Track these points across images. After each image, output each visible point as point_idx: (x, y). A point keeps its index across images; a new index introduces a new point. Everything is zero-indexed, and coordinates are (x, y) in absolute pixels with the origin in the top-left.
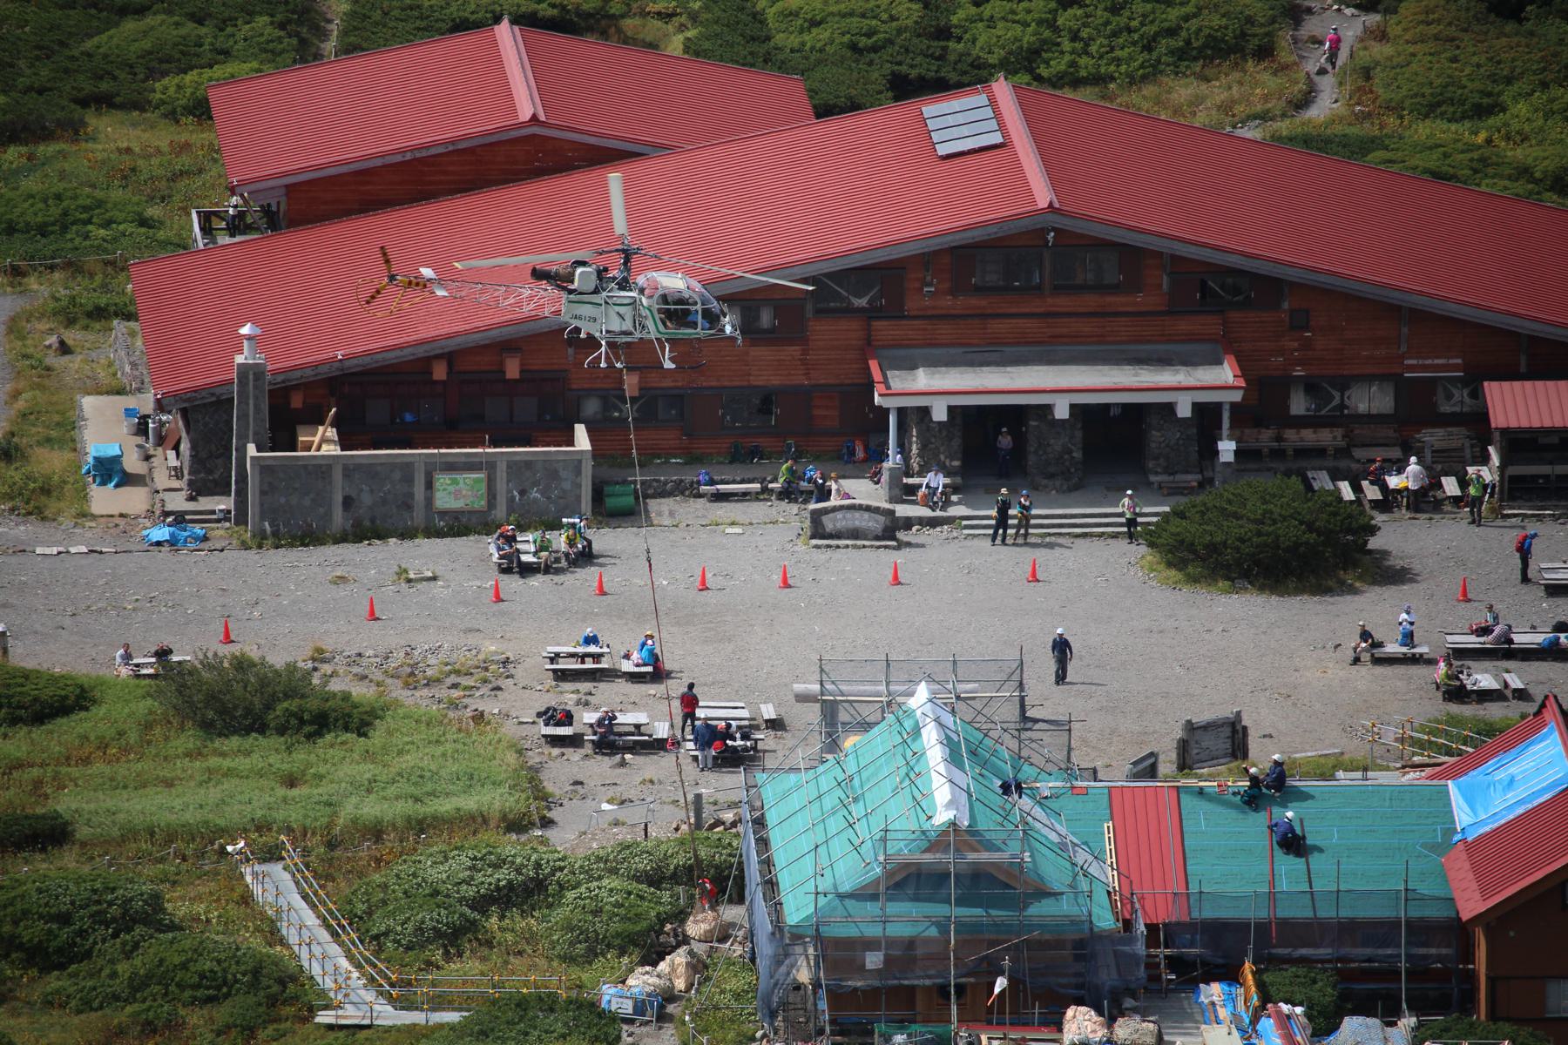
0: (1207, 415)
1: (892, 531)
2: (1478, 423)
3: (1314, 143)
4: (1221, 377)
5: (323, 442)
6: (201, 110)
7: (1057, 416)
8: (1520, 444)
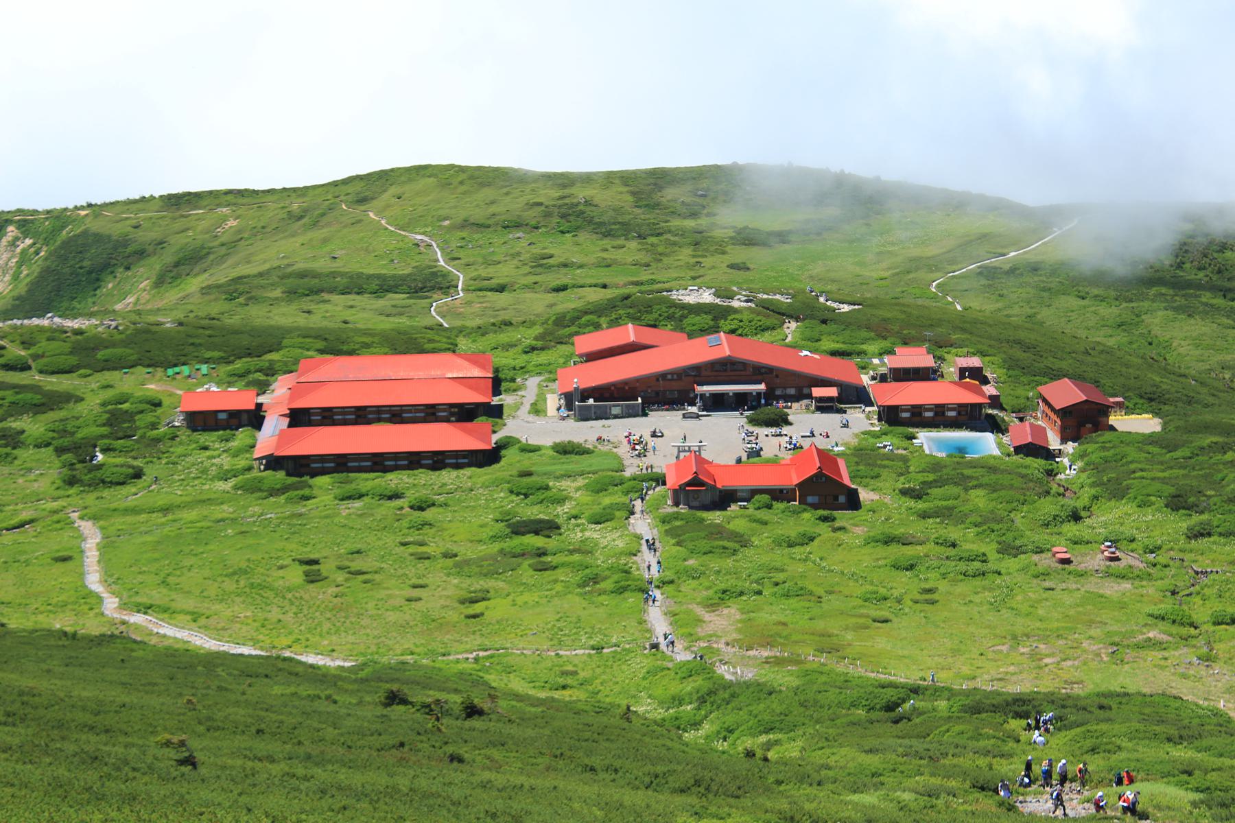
0: (759, 394)
1: (698, 417)
2: (810, 396)
3: (787, 346)
4: (762, 387)
5: (591, 401)
6: (573, 344)
7: (1158, 429)
8: (820, 400)
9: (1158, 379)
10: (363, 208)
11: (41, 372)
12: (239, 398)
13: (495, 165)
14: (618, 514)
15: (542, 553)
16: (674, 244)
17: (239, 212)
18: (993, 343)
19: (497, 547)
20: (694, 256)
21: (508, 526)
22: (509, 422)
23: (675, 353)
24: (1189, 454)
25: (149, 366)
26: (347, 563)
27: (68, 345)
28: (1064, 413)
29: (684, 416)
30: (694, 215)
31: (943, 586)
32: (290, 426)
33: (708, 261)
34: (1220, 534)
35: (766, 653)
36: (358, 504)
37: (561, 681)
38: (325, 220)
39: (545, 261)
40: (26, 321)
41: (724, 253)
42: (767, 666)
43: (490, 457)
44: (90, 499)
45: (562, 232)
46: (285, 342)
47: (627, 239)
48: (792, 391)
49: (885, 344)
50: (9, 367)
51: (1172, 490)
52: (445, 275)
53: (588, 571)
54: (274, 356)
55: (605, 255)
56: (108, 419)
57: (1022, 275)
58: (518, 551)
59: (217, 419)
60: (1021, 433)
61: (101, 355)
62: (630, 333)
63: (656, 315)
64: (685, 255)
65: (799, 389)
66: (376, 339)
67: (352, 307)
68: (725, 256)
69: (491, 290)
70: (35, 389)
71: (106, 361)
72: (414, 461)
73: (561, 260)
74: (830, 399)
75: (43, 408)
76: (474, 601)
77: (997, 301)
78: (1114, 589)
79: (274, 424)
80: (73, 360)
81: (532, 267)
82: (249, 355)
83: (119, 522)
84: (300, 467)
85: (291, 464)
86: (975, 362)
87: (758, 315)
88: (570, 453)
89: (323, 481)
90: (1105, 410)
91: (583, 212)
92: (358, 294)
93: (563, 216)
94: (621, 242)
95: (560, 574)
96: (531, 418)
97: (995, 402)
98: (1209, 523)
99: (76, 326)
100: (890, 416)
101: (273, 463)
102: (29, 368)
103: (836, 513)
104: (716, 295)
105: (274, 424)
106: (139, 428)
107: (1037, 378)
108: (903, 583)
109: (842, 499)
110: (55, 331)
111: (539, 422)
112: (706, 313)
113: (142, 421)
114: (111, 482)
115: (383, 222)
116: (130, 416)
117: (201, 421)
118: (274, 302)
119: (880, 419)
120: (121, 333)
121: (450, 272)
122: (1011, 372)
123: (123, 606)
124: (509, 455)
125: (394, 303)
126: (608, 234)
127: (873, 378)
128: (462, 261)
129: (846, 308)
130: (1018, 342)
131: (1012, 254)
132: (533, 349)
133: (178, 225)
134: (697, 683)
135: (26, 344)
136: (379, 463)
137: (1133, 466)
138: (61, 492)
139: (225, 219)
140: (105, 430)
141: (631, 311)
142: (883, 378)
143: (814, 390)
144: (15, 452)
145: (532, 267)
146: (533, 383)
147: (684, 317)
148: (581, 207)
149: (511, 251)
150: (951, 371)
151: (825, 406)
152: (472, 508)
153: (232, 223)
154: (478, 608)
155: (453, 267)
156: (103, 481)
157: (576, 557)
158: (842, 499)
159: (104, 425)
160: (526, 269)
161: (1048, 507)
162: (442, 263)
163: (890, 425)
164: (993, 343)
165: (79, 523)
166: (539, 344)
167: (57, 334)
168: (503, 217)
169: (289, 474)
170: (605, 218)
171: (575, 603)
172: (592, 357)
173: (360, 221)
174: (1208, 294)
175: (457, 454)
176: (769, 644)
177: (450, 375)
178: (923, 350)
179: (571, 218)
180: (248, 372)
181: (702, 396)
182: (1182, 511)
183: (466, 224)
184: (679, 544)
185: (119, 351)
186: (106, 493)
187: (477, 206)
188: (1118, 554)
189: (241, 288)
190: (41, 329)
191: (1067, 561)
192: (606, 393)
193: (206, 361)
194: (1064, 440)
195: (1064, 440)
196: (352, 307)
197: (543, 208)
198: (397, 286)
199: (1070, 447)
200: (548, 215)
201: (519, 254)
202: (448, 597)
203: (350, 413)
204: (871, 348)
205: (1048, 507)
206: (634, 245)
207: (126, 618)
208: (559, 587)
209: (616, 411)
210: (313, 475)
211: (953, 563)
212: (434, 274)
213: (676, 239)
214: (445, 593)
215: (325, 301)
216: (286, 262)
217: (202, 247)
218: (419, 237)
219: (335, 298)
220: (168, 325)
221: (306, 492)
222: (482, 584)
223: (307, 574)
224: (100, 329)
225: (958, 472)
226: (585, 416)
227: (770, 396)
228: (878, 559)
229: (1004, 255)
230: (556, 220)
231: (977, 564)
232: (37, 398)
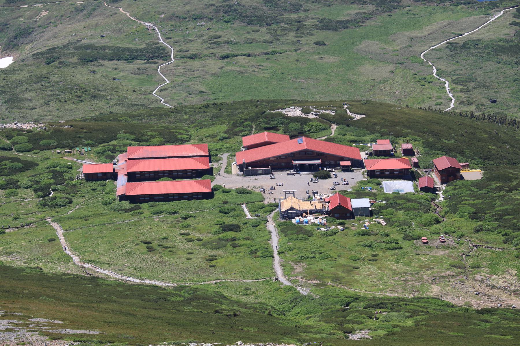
0: (319, 165)
1: (293, 174)
4: (319, 161)
5: (250, 168)
8: (343, 166)
10: (116, 5)
11: (18, 151)
12: (107, 168)
14: (262, 222)
15: (234, 239)
16: (286, 29)
17: (48, 7)
19: (217, 237)
20: (296, 37)
21: (221, 227)
22: (217, 176)
23: (285, 146)
24: (486, 192)
26: (162, 243)
29: (288, 174)
30: (296, 11)
31: (381, 254)
33: (304, 40)
34: (485, 230)
35: (315, 282)
36: (161, 216)
37: (245, 292)
38: (96, 13)
39: (216, 40)
41: (312, 35)
42: (314, 287)
44: (53, 212)
45: (226, 22)
46: (118, 136)
47: (260, 26)
48: (333, 163)
49: (373, 136)
50: (4, 149)
51: (473, 210)
52: (164, 49)
53: (252, 248)
54: (114, 143)
55: (249, 36)
56: (52, 175)
57: (469, 48)
58: (225, 238)
60: (423, 182)
61: (42, 142)
62: (265, 136)
63: (276, 122)
64: (292, 36)
65: (336, 162)
66: (156, 133)
67: (116, 69)
68: (313, 37)
69: (189, 58)
70: (18, 160)
71: (44, 146)
72: (180, 197)
73: (226, 39)
74: (348, 166)
75: (23, 169)
76: (211, 260)
77: (454, 65)
78: (441, 253)
79: (122, 180)
80: (30, 146)
81: (210, 44)
82: (104, 142)
83: (69, 223)
84: (136, 200)
86: (409, 146)
87: (320, 122)
88: (243, 193)
89: (144, 205)
90: (458, 170)
91: (236, 10)
92: (118, 60)
93: (226, 12)
94: (257, 27)
95: (242, 249)
96: (226, 175)
97: (416, 165)
98: (482, 226)
99: (28, 128)
101: (123, 198)
102: (12, 149)
103: (346, 221)
104: (303, 111)
105: (122, 180)
106: (66, 180)
107: (437, 151)
108: (368, 253)
109: (348, 215)
110: (20, 130)
111: (229, 177)
112: (297, 122)
113: (67, 176)
114: (60, 205)
115: (128, 14)
116: (60, 174)
117: (91, 177)
118: (75, 65)
119: (367, 175)
120: (47, 131)
121: (166, 47)
122: (426, 149)
123: (82, 260)
124: (218, 195)
125: (138, 66)
126: (250, 23)
127: (367, 154)
128: (172, 40)
130: (432, 133)
131: (466, 34)
132: (224, 138)
133: (14, 15)
134: (289, 296)
135: (9, 137)
136: (167, 198)
137: (463, 198)
138: (40, 210)
139: (40, 11)
140: (52, 181)
141: (265, 120)
143: (341, 162)
144: (17, 190)
145: (210, 44)
146: (225, 156)
147: (288, 123)
148: (235, 7)
149: (199, 33)
150: (400, 152)
151: (346, 169)
152: (205, 220)
153: (44, 13)
154: (213, 263)
155: (168, 43)
156: (57, 205)
157: (248, 242)
158: (348, 215)
159: (51, 178)
160: (207, 45)
161: (426, 217)
162: (162, 41)
163: (371, 178)
165: (52, 223)
166: (226, 135)
168: (193, 13)
170: (248, 14)
171: (249, 261)
172: (249, 148)
173: (115, 14)
175: (197, 194)
176: (316, 279)
178: (388, 141)
179: (230, 13)
180: (105, 151)
181: (296, 165)
182: (475, 220)
183: (173, 17)
184: (285, 236)
186: (59, 209)
187: (179, 6)
188: (445, 240)
189: (55, 55)
191: (427, 243)
192: (256, 164)
193: (86, 145)
194: (442, 183)
195: (442, 183)
196: (116, 69)
197: (214, 7)
198: (138, 56)
199: (443, 187)
200: (217, 11)
201: (202, 36)
202: (201, 258)
204: (368, 138)
205: (426, 217)
206: (264, 29)
207: (84, 265)
208: (242, 254)
209: (260, 172)
210: (141, 202)
211: (385, 244)
212: (158, 48)
213: (287, 26)
214: (200, 256)
215: (101, 65)
216: (76, 38)
217: (29, 28)
218: (148, 24)
219: (106, 63)
221: (139, 211)
222: (214, 252)
223: (148, 248)
224: (38, 130)
225: (397, 200)
226: (248, 174)
227: (323, 165)
228: (359, 242)
229: (461, 35)
230: (222, 14)
231: (394, 244)
232: (20, 165)
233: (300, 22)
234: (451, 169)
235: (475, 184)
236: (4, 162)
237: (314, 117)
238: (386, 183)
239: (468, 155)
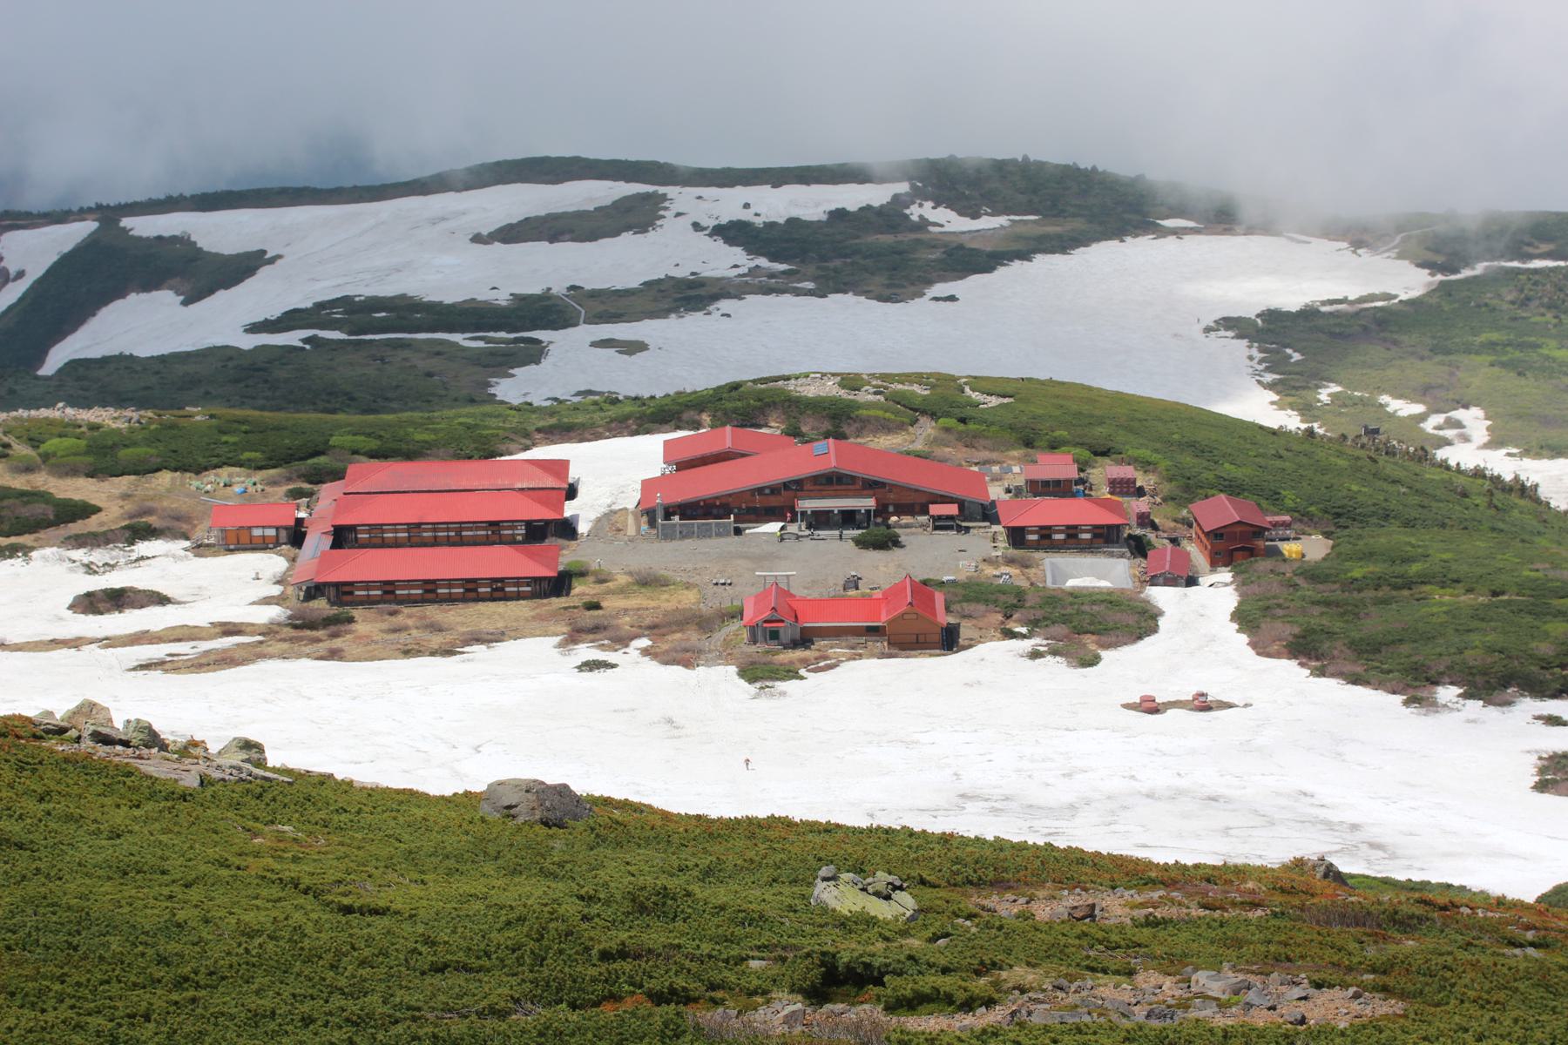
0: (868, 512)
5: (676, 518)
8: (940, 518)
9: (1355, 488)
13: (632, 158)
18: (1158, 445)
20: (888, 286)
25: (175, 470)
27: (83, 443)
28: (1216, 534)
32: (332, 547)
39: (692, 293)
40: (33, 412)
43: (559, 585)
59: (251, 537)
85: (333, 592)
97: (1145, 520)
99: (93, 419)
100: (1017, 536)
104: (842, 385)
110: (67, 425)
127: (1008, 491)
129: (994, 401)
130: (1192, 445)
135: (34, 442)
142: (1018, 492)
151: (941, 524)
164: (1158, 445)
167: (70, 429)
169: (332, 604)
174: (1553, 343)
177: (519, 485)
185: (141, 451)
190: (50, 422)
203: (403, 531)
220: (198, 418)
227: (882, 511)
233: (900, 253)
234: (1238, 529)
235: (1313, 574)
236: (6, 503)
237: (871, 397)
238: (1052, 564)
239: (1292, 505)
